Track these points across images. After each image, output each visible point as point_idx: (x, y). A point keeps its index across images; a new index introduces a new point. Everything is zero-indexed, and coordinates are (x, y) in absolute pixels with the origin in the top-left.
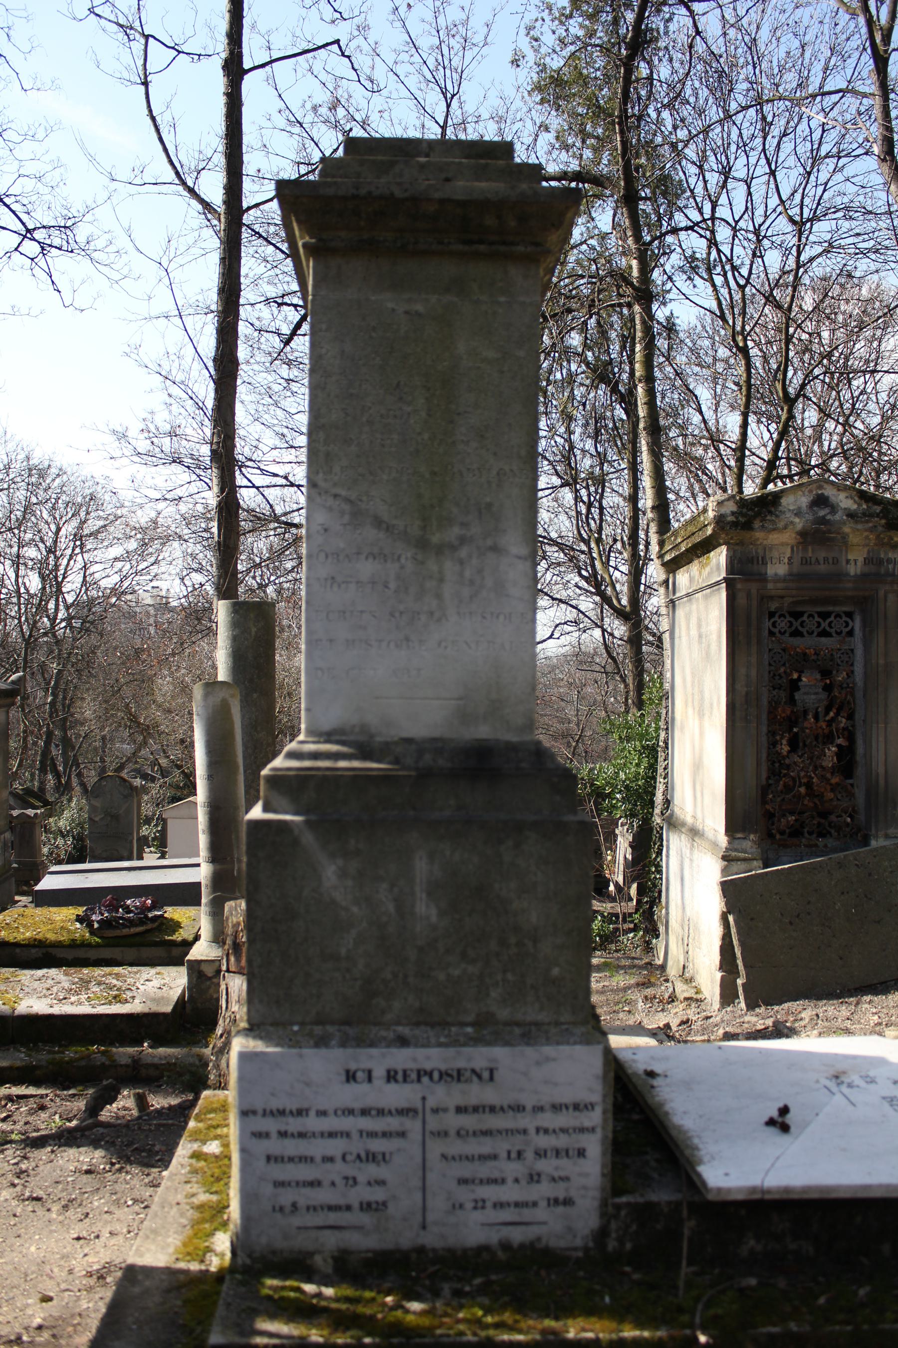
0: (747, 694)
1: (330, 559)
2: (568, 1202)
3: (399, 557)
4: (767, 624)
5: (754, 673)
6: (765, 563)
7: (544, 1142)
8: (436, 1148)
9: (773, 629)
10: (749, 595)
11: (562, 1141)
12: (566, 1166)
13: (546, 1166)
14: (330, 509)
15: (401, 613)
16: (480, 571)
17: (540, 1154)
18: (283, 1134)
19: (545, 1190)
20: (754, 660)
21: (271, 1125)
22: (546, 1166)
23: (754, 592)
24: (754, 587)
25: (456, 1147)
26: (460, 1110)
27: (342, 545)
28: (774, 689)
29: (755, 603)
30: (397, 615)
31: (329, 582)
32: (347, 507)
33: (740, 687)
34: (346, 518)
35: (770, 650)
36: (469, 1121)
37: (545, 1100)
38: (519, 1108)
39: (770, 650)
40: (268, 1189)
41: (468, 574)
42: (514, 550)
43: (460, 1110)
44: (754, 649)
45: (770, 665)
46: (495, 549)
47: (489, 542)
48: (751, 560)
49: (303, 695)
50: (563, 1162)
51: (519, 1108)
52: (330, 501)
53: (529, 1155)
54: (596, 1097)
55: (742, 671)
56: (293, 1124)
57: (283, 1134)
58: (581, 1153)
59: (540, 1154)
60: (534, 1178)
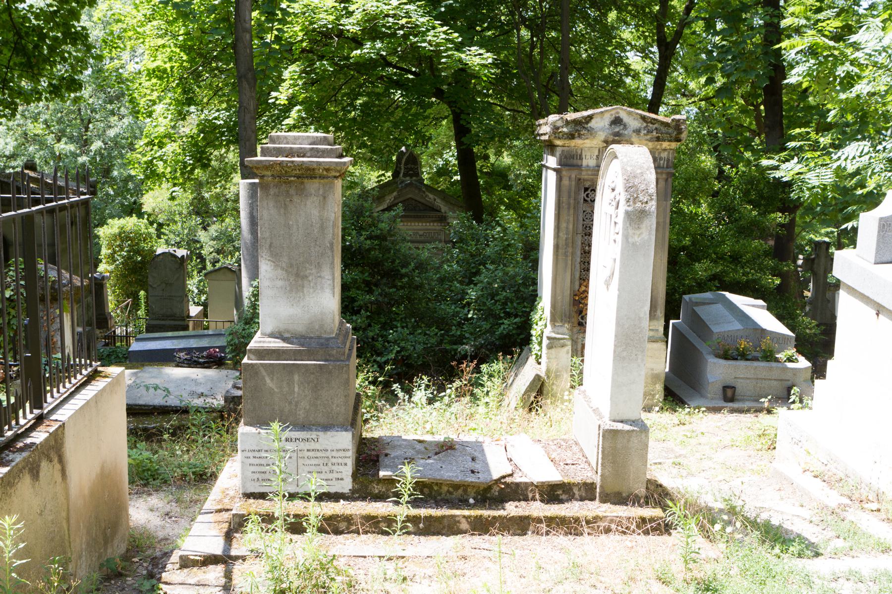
0: (566, 239)
2: (342, 479)
5: (571, 226)
6: (581, 159)
7: (334, 460)
8: (301, 461)
10: (570, 178)
11: (340, 461)
12: (341, 468)
13: (335, 468)
16: (316, 284)
17: (333, 464)
18: (254, 457)
19: (335, 475)
20: (571, 219)
21: (251, 454)
22: (334, 468)
23: (573, 176)
24: (574, 174)
25: (308, 462)
26: (308, 450)
29: (573, 183)
36: (311, 454)
37: (335, 448)
38: (327, 450)
40: (250, 474)
43: (308, 450)
44: (572, 211)
46: (320, 277)
48: (572, 157)
50: (340, 467)
51: (327, 450)
53: (330, 464)
54: (350, 448)
55: (563, 225)
56: (257, 454)
57: (254, 457)
58: (346, 464)
59: (333, 464)
60: (331, 472)
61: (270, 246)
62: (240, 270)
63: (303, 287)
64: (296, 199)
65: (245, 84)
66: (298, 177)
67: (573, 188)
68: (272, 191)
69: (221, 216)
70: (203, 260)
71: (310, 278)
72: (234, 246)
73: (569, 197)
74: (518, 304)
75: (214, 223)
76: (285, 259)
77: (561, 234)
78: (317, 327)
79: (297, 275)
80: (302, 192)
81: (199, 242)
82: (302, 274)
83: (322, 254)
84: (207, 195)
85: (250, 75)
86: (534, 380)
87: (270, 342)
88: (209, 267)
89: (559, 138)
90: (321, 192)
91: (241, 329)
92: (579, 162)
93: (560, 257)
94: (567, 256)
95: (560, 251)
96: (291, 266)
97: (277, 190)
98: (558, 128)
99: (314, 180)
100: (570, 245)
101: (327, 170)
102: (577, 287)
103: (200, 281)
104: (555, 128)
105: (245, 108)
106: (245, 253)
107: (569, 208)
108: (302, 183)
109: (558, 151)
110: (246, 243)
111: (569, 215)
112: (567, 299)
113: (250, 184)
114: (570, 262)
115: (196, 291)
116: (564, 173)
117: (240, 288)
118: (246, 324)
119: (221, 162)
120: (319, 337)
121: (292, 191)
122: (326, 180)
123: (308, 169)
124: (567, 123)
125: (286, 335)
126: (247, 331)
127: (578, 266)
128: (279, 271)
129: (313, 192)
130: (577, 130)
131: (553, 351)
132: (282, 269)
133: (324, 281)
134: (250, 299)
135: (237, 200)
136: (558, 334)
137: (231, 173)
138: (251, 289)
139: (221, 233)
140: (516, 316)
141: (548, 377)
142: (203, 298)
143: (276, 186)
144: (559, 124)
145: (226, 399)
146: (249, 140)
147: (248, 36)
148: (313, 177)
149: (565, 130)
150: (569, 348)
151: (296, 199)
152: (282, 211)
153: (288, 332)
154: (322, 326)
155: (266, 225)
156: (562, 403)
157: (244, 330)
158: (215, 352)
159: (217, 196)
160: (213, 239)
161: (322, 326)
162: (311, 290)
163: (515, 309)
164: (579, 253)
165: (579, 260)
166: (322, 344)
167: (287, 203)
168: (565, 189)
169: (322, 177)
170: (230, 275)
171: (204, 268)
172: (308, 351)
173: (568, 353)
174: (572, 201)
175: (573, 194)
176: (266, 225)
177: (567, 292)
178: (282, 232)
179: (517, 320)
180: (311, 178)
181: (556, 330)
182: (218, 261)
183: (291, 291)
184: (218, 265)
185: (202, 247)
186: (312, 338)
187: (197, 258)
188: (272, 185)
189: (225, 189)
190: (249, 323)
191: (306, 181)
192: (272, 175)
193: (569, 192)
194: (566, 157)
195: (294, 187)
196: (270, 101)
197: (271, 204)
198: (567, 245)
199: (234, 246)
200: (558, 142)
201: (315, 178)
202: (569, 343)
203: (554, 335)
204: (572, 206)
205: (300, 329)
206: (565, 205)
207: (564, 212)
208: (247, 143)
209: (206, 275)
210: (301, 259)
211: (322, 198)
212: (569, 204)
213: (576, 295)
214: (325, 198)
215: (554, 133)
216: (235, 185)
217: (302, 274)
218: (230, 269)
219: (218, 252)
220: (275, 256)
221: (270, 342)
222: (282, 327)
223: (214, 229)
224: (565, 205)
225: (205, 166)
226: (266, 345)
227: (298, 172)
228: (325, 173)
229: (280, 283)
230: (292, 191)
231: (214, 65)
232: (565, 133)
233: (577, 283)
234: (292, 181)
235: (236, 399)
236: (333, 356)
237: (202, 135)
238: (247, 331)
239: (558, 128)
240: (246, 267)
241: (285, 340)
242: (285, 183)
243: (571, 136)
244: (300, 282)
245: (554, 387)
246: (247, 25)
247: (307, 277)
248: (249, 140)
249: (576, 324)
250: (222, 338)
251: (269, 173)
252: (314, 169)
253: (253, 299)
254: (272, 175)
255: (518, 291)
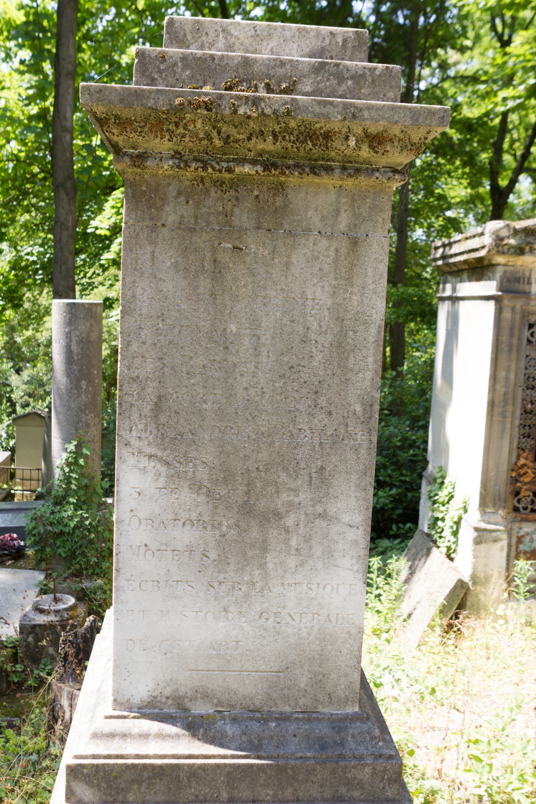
0: (505, 394)
1: (143, 527)
3: (220, 524)
4: (526, 334)
5: (512, 376)
9: (531, 339)
10: (513, 309)
14: (144, 470)
15: (220, 583)
16: (307, 539)
20: (513, 366)
24: (519, 304)
27: (157, 511)
28: (528, 389)
29: (518, 317)
30: (215, 585)
31: (143, 549)
32: (163, 469)
33: (500, 388)
34: (162, 482)
35: (527, 356)
39: (527, 356)
41: (294, 542)
42: (346, 518)
44: (514, 355)
45: (526, 368)
46: (323, 516)
47: (319, 509)
48: (518, 280)
49: (88, 83)
52: (144, 462)
55: (502, 374)
61: (157, 407)
62: (50, 417)
63: (264, 549)
64: (253, 243)
65: (63, 195)
66: (268, 166)
67: (517, 324)
68: (171, 214)
69: (33, 361)
70: (13, 405)
71: (290, 521)
72: (45, 391)
73: (511, 335)
74: (393, 470)
75: (26, 368)
76: (208, 454)
77: (498, 387)
78: (303, 682)
79: (247, 510)
80: (275, 218)
81: (9, 385)
82: (262, 505)
83: (336, 441)
84: (19, 340)
85: (69, 184)
86: (455, 587)
87: (144, 736)
88: (19, 410)
89: (503, 253)
90: (343, 223)
91: (49, 511)
92: (527, 288)
93: (495, 419)
94: (505, 417)
95: (496, 409)
96: (228, 477)
97: (187, 211)
98: (502, 239)
99: (325, 180)
100: (511, 401)
101: (376, 141)
102: (514, 459)
103: (8, 426)
104: (499, 239)
105: (62, 224)
106: (58, 402)
107: (510, 351)
108: (280, 188)
109: (499, 272)
110: (59, 389)
111: (510, 361)
112: (503, 476)
113: (68, 304)
114: (508, 425)
115: (5, 435)
116: (506, 302)
117: (49, 437)
118: (56, 504)
119: (34, 304)
120: (310, 716)
121: (243, 217)
122: (363, 181)
123: (308, 134)
124: (516, 232)
125: (201, 709)
126: (57, 516)
127: (516, 430)
128: (186, 495)
129: (315, 221)
130: (528, 243)
131: (482, 547)
132: (197, 487)
133: (335, 529)
134: (62, 469)
135: (49, 344)
136: (489, 523)
137: (44, 316)
138: (65, 455)
139: (32, 378)
140: (391, 486)
141: (475, 583)
142: (12, 443)
143: (186, 194)
144: (504, 233)
145: (23, 629)
146: (65, 263)
147: (68, 137)
148: (317, 167)
149: (512, 241)
150: (504, 543)
151: (253, 243)
152: (205, 284)
153: (206, 696)
154: (319, 680)
155: (146, 333)
156: (495, 621)
157: (53, 513)
158: (13, 539)
159: (28, 339)
160: (26, 384)
161: (319, 680)
162: (292, 562)
163: (390, 476)
164: (518, 412)
165: (517, 422)
166: (323, 745)
167: (224, 257)
168: (506, 325)
169: (352, 168)
170: (39, 421)
171: (14, 411)
172: (280, 770)
173: (502, 550)
174: (515, 342)
175: (516, 332)
176: (146, 333)
177: (504, 467)
178: (201, 360)
179: (394, 491)
180: (314, 171)
181: (486, 518)
182: (28, 405)
183: (223, 561)
184: (28, 410)
185: (12, 391)
186: (284, 718)
187: (7, 402)
188: (172, 191)
189: (37, 331)
190: (60, 504)
191: (293, 179)
192: (177, 155)
193: (512, 328)
194: (509, 281)
195: (248, 203)
196: (89, 231)
197: (167, 258)
198: (505, 401)
199: (45, 391)
200: (500, 259)
201: (329, 170)
202: (505, 536)
203: (483, 525)
204: (515, 348)
205: (247, 685)
206: (504, 347)
207: (504, 356)
208: (64, 267)
209: (14, 420)
210: (264, 455)
211: (344, 245)
212: (510, 346)
213: (513, 470)
214: (355, 243)
215: (497, 246)
216: (47, 330)
217: (262, 505)
218: (39, 415)
219: (30, 395)
220: (173, 443)
221: (144, 736)
222: (186, 681)
223: (26, 375)
224: (504, 347)
225: (16, 306)
226: (131, 748)
227: (268, 145)
228: (365, 152)
229: (185, 536)
230: (243, 217)
231: (26, 203)
232: (511, 247)
233: (515, 454)
234: (244, 179)
235: (38, 629)
236: (361, 785)
237: (13, 272)
238: (57, 516)
239: (502, 239)
240: (59, 423)
241: (196, 727)
242: (219, 184)
243: (520, 251)
244: (255, 533)
245: (482, 597)
246: (68, 124)
247: (278, 515)
248: (65, 263)
249: (511, 510)
250: (22, 515)
251: (164, 146)
252: (327, 136)
253: (67, 470)
254: (177, 155)
255: (395, 455)
